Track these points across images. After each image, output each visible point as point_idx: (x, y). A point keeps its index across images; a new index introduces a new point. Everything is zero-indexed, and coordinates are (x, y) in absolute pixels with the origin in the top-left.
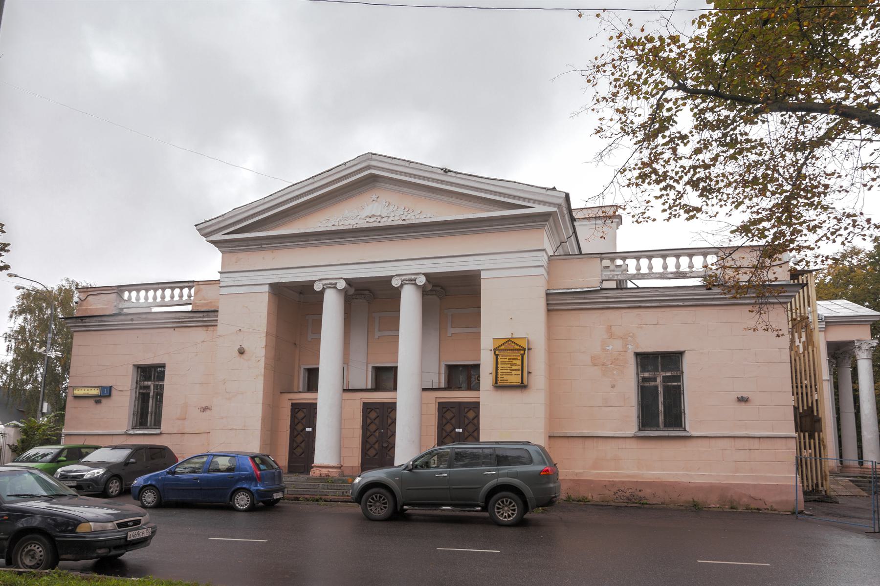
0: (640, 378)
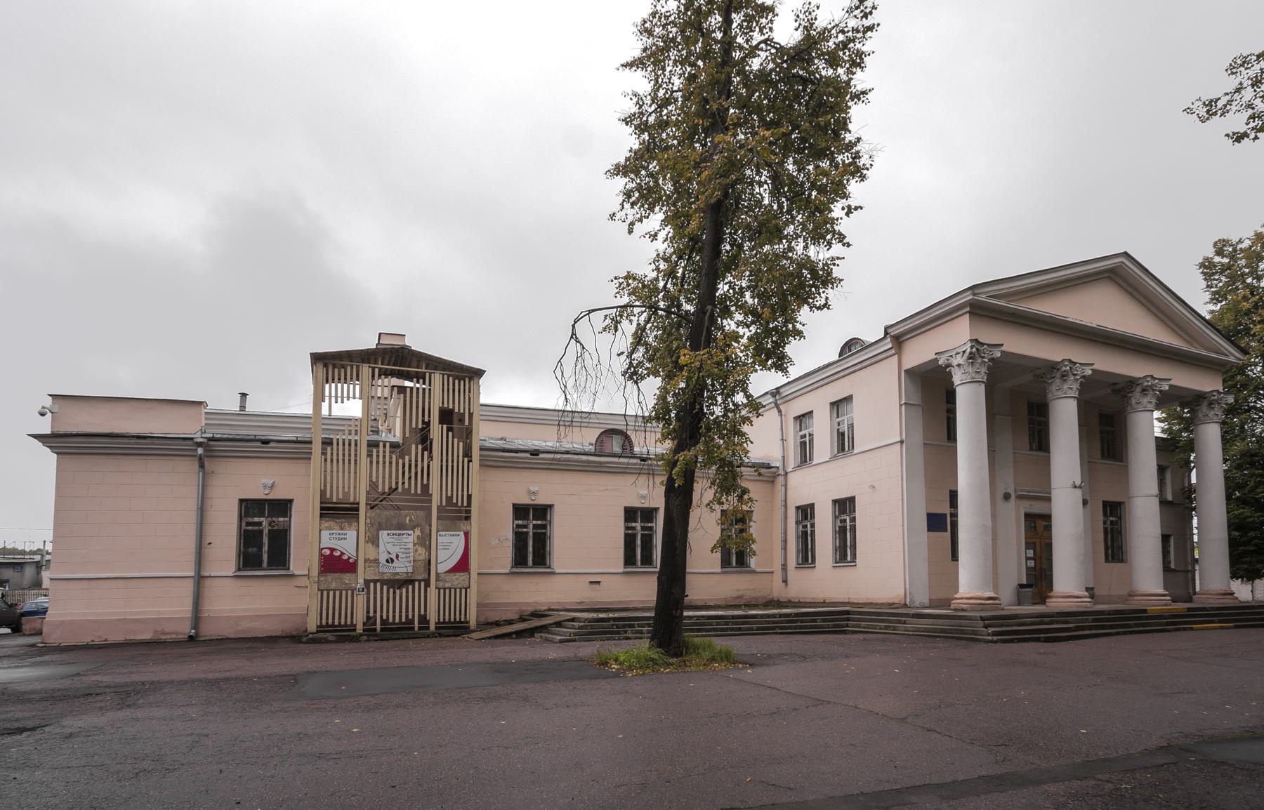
0: (515, 526)
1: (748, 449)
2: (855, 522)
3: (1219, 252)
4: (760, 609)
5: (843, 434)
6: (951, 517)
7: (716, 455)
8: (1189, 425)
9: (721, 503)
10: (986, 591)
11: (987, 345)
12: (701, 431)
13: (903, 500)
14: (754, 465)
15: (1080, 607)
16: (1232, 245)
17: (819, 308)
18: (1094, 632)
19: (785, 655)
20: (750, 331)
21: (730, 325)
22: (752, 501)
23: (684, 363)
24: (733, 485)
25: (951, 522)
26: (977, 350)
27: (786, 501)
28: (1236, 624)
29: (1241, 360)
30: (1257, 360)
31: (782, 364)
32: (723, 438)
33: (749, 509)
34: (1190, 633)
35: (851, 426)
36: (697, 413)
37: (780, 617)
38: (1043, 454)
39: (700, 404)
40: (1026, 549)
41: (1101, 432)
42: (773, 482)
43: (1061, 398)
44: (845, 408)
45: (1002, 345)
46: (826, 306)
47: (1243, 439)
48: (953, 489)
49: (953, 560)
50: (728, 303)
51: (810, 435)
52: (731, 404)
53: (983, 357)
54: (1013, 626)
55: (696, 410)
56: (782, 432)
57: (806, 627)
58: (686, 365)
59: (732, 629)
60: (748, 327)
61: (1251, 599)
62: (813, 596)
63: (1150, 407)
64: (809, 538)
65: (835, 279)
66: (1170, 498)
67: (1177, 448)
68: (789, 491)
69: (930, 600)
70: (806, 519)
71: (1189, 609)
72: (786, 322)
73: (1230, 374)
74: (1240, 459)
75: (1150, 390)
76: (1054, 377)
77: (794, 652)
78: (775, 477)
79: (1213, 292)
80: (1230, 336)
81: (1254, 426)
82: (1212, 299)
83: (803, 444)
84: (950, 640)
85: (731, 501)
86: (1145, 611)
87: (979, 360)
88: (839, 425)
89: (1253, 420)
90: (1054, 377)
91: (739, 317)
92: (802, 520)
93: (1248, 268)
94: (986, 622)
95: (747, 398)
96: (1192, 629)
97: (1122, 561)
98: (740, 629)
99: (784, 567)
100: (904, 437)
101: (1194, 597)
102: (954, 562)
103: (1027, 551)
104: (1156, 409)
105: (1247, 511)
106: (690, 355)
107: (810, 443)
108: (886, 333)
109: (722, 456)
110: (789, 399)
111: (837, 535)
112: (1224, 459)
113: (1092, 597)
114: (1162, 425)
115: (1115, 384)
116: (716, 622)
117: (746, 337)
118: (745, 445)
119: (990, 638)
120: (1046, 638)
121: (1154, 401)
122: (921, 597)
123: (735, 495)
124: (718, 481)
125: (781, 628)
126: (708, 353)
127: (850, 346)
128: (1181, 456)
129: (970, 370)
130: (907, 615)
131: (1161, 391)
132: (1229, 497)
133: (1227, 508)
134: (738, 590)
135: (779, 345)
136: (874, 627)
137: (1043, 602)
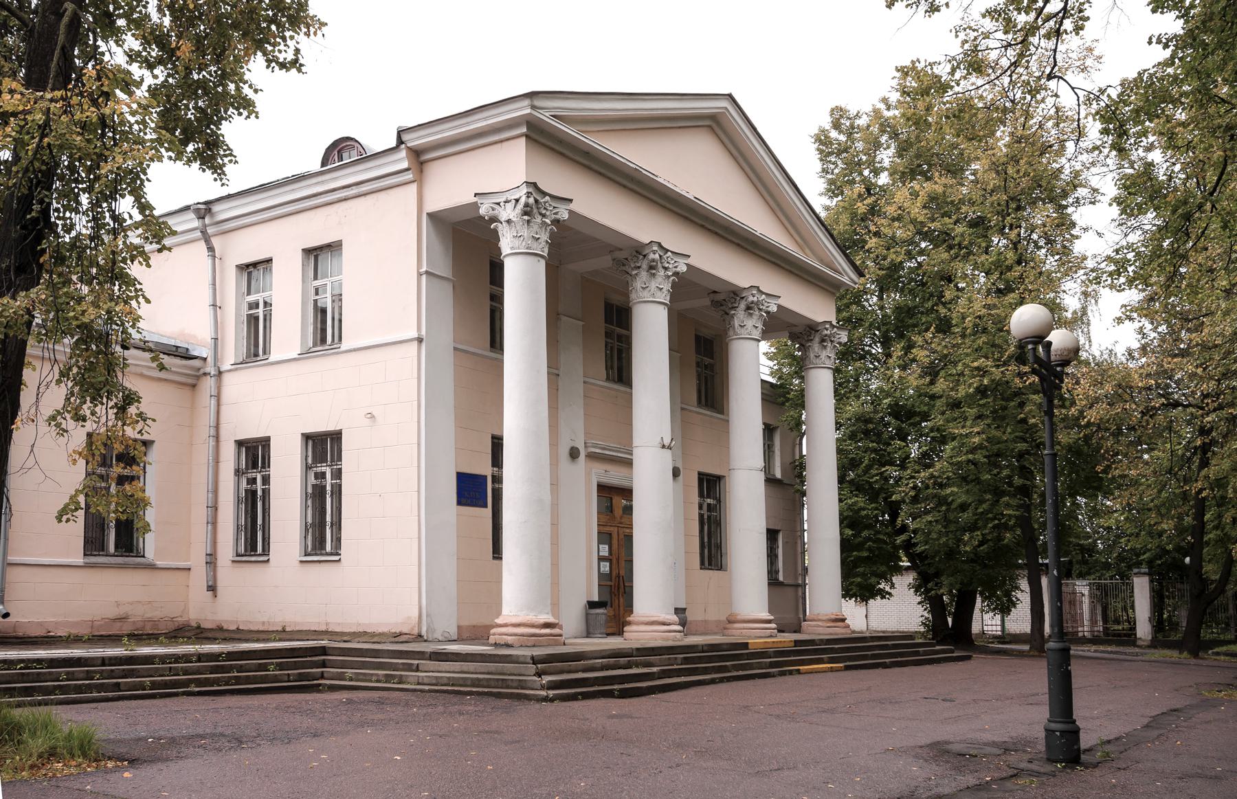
1: (140, 312)
2: (340, 479)
3: (836, 125)
4: (162, 644)
5: (324, 311)
6: (493, 482)
7: (72, 314)
8: (801, 367)
9: (81, 419)
10: (540, 613)
11: (550, 196)
12: (41, 260)
13: (419, 445)
14: (144, 347)
15: (667, 639)
16: (850, 119)
17: (283, 66)
18: (683, 679)
19: (202, 737)
20: (155, 77)
21: (115, 54)
22: (145, 420)
23: (10, 109)
24: (106, 383)
25: (493, 490)
26: (536, 201)
27: (217, 427)
28: (848, 663)
29: (856, 283)
30: (873, 287)
31: (213, 157)
32: (89, 283)
33: (138, 436)
34: (797, 677)
35: (338, 298)
36: (35, 221)
37: (199, 660)
38: (622, 388)
39: (41, 202)
40: (599, 543)
41: (698, 364)
42: (194, 386)
43: (645, 302)
44: (326, 260)
45: (571, 201)
46: (295, 64)
47: (858, 397)
48: (497, 433)
49: (494, 558)
50: (111, 8)
51: (265, 303)
52: (107, 215)
53: (544, 216)
54: (577, 671)
55: (34, 214)
56: (215, 290)
57: (248, 680)
58: (15, 114)
59: (100, 688)
60: (150, 67)
61: (866, 629)
62: (265, 619)
63: (756, 334)
64: (259, 504)
65: (312, 18)
66: (778, 475)
67: (788, 400)
68: (223, 409)
69: (459, 627)
70: (255, 466)
71: (797, 643)
72: (224, 77)
73: (845, 301)
74: (854, 425)
75: (756, 309)
76: (639, 267)
77: (219, 730)
78: (198, 377)
79: (829, 179)
80: (848, 246)
81: (869, 380)
82: (828, 190)
83: (253, 320)
84: (485, 699)
85: (103, 415)
86: (745, 645)
87: (538, 219)
88: (317, 294)
89: (868, 371)
90: (639, 267)
91: (132, 43)
92: (247, 468)
93: (865, 155)
94: (539, 666)
95: (142, 212)
96: (798, 672)
97: (720, 568)
98: (117, 687)
99: (211, 560)
100: (423, 332)
101: (803, 623)
102: (496, 562)
103: (601, 546)
104: (763, 339)
105: (860, 501)
106: (22, 94)
107: (265, 320)
108: (400, 142)
109: (86, 320)
110: (230, 228)
111: (309, 502)
112: (837, 423)
113: (683, 623)
114: (771, 363)
115: (715, 292)
116: (67, 673)
117: (145, 87)
118: (134, 303)
119: (543, 693)
120: (620, 690)
121: (760, 326)
122: (444, 624)
123: (111, 404)
124: (75, 370)
125: (199, 683)
126: (62, 98)
127: (339, 150)
128: (792, 413)
129: (525, 232)
130: (420, 655)
131: (768, 313)
132: (841, 480)
133: (839, 494)
134: (118, 604)
135: (211, 118)
136: (367, 678)
137: (620, 633)
